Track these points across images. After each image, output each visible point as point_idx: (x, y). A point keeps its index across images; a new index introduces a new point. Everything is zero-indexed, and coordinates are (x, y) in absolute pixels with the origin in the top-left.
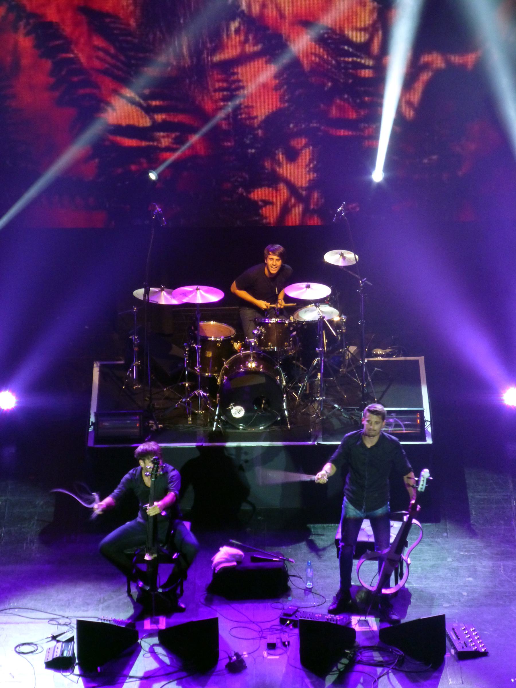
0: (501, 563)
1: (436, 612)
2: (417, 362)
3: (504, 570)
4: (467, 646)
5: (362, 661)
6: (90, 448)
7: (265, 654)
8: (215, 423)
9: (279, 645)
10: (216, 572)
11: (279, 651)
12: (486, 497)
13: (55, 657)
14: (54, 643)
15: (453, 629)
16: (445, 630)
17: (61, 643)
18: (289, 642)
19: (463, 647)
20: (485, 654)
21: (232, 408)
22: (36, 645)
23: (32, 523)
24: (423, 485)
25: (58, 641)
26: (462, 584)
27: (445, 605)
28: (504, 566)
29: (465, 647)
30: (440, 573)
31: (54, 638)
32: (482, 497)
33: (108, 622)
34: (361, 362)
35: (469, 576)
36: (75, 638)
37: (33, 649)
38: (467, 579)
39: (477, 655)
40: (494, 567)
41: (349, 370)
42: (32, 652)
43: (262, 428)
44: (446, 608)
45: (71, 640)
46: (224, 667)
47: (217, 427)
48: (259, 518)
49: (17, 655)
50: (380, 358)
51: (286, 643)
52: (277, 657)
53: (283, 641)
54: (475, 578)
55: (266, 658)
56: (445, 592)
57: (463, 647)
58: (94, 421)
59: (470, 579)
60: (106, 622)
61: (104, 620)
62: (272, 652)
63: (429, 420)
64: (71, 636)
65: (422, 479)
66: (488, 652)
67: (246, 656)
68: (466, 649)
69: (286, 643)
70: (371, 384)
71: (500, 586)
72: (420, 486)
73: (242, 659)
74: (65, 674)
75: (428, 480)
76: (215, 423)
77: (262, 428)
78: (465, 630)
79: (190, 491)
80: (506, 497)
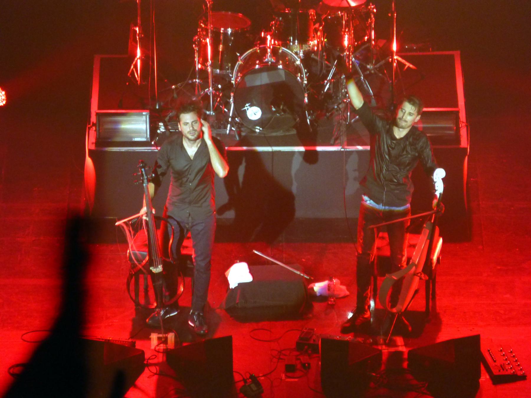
4: (503, 370)
8: (229, 126)
15: (489, 351)
18: (309, 364)
19: (499, 371)
20: (523, 378)
29: (501, 370)
39: (515, 378)
47: (231, 130)
52: (296, 380)
57: (499, 371)
59: (508, 296)
63: (464, 120)
68: (502, 373)
76: (229, 126)
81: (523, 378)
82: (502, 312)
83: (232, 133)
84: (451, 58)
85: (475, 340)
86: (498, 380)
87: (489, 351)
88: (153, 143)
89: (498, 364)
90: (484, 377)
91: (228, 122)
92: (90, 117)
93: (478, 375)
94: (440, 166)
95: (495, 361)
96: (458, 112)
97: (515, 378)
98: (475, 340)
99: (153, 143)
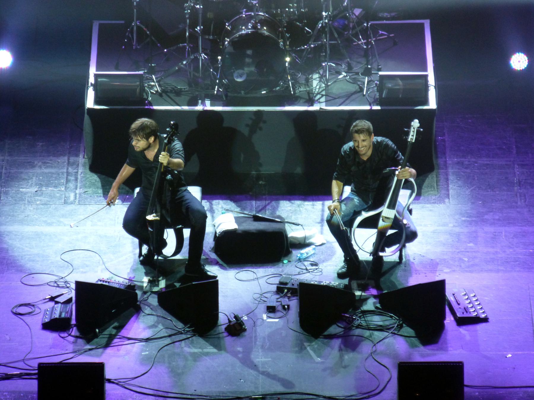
0: (503, 229)
1: (438, 278)
2: (422, 25)
3: (506, 236)
4: (467, 312)
5: (361, 326)
6: (90, 110)
7: (265, 316)
8: (217, 87)
9: (280, 308)
10: (217, 235)
11: (279, 314)
12: (488, 162)
13: (53, 318)
14: (52, 304)
15: (453, 294)
16: (444, 295)
17: (60, 304)
18: (288, 306)
19: (463, 313)
20: (485, 320)
21: (234, 72)
22: (33, 306)
23: (30, 184)
24: (413, 136)
25: (57, 303)
26: (463, 250)
27: (445, 271)
28: (506, 232)
29: (465, 313)
30: (437, 231)
31: (52, 299)
32: (486, 162)
33: (107, 284)
34: (365, 24)
35: (470, 242)
36: (74, 299)
37: (30, 310)
38: (468, 245)
39: (477, 320)
40: (495, 233)
41: (354, 32)
42: (21, 305)
43: (265, 92)
44: (446, 273)
45: (69, 301)
46: (223, 330)
47: (218, 90)
48: (260, 183)
49: (14, 316)
50: (385, 22)
51: (286, 307)
52: (277, 320)
53: (283, 304)
54: (476, 244)
55: (265, 320)
56: (445, 257)
57: (463, 313)
58: (93, 83)
59: (471, 245)
60: (104, 283)
61: (103, 281)
62: (271, 315)
64: (70, 297)
65: (412, 129)
66: (488, 319)
67: (246, 318)
68: (466, 315)
69: (286, 307)
70: (375, 47)
71: (501, 252)
72: (410, 137)
73: (242, 321)
74: (62, 335)
75: (418, 131)
77: (265, 92)
78: (465, 295)
79: (195, 158)
80: (509, 163)
81: (485, 320)
82: (466, 259)
83: (220, 94)
84: (421, 27)
85: (441, 284)
86: (462, 322)
87: (453, 294)
88: (286, 291)
89: (462, 306)
90: (449, 320)
91: (216, 84)
92: (88, 78)
93: (443, 317)
94: (508, 58)
95: (459, 304)
96: (426, 76)
97: (477, 320)
98: (441, 284)
99: (286, 291)
